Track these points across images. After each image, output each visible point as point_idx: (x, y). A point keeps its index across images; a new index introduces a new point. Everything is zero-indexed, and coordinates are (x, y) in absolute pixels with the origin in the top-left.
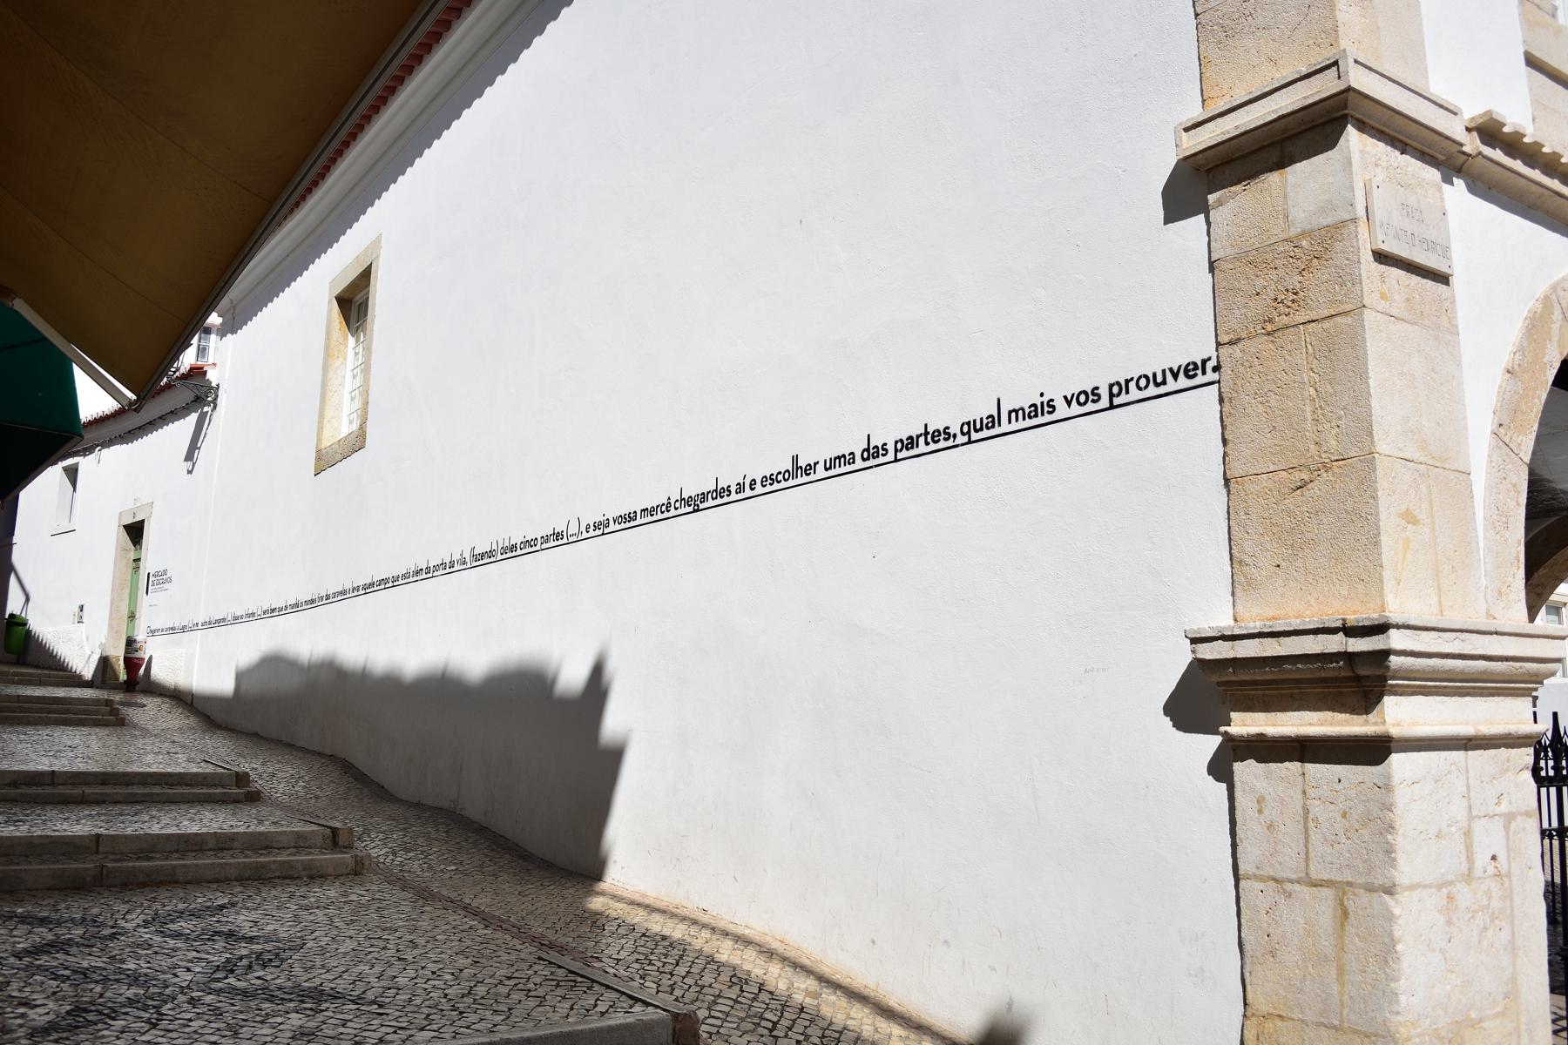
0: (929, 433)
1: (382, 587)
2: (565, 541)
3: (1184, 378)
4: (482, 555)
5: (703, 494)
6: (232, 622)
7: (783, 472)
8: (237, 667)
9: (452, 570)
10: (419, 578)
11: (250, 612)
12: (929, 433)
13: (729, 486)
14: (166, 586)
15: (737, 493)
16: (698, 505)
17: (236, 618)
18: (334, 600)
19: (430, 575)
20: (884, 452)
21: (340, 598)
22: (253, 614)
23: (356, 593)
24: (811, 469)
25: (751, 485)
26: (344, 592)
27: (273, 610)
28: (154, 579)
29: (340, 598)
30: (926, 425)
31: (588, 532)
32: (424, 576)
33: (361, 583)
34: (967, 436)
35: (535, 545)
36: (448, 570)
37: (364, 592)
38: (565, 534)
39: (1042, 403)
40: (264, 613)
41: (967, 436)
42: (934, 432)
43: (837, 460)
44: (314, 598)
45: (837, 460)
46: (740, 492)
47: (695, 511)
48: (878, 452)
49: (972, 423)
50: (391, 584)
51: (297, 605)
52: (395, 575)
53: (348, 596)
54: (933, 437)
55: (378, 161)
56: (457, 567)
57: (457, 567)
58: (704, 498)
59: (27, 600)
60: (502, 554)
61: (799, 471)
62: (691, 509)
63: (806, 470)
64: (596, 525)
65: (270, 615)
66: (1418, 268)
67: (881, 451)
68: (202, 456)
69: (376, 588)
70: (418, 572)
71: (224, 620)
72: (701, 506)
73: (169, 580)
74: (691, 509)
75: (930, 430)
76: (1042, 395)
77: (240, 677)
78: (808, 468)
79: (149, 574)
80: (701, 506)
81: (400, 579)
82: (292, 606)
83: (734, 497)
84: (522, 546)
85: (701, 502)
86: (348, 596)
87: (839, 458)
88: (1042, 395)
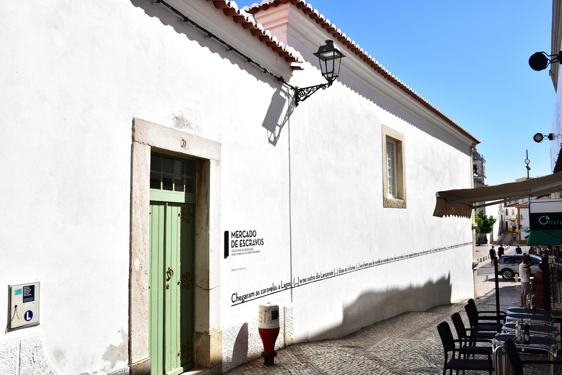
1: (415, 256)
2: (334, 275)
4: (435, 250)
5: (245, 295)
6: (339, 274)
8: (344, 304)
9: (374, 265)
10: (425, 254)
11: (352, 266)
14: (256, 248)
15: (256, 295)
16: (244, 300)
18: (398, 260)
19: (426, 253)
21: (401, 259)
22: (354, 268)
23: (407, 257)
25: (301, 281)
26: (402, 257)
27: (366, 265)
28: (234, 239)
29: (401, 259)
31: (301, 283)
32: (425, 254)
33: (409, 254)
35: (314, 279)
36: (430, 253)
37: (409, 257)
40: (361, 267)
46: (246, 298)
47: (243, 302)
48: (275, 288)
50: (417, 255)
51: (379, 262)
52: (370, 262)
53: (404, 258)
55: (381, 90)
56: (431, 252)
57: (431, 252)
58: (246, 297)
60: (339, 273)
62: (241, 302)
64: (258, 294)
65: (364, 267)
68: (550, 149)
69: (413, 256)
70: (424, 252)
72: (245, 300)
73: (261, 242)
74: (241, 302)
77: (346, 311)
79: (226, 233)
80: (245, 300)
81: (344, 271)
82: (377, 262)
83: (394, 260)
84: (262, 292)
85: (245, 299)
86: (404, 258)
87: (252, 293)
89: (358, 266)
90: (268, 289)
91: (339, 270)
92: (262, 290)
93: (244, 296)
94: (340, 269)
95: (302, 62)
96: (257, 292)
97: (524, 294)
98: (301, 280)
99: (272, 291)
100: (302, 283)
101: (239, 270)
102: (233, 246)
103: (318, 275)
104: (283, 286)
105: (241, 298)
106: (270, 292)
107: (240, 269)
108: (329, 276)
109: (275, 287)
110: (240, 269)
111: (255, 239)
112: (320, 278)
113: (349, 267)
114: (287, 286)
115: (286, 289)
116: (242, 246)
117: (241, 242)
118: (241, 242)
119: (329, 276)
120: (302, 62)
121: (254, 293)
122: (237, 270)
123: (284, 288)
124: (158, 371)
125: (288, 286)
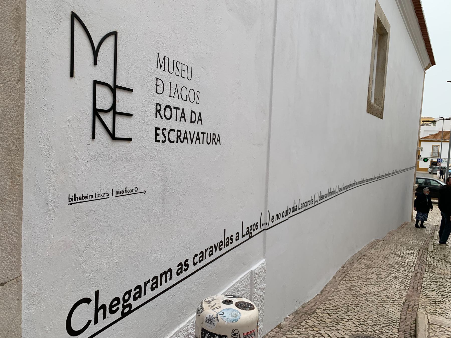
0: (83, 197)
3: (234, 305)
5: (156, 278)
7: (256, 229)
11: (332, 191)
12: (83, 197)
13: (187, 260)
17: (321, 197)
20: (186, 268)
24: (86, 197)
30: (83, 195)
34: (70, 198)
38: (259, 224)
39: (119, 191)
41: (70, 198)
42: (85, 197)
43: (164, 276)
44: (362, 180)
45: (164, 276)
48: (228, 242)
49: (74, 200)
54: (85, 198)
59: (187, 88)
61: (77, 198)
63: (79, 198)
64: (230, 241)
66: (384, 81)
67: (184, 267)
71: (312, 201)
75: (84, 196)
76: (88, 194)
78: (221, 244)
84: (197, 259)
87: (165, 273)
88: (88, 194)
89: (316, 199)
90: (212, 247)
91: (319, 196)
92: (196, 255)
93: (133, 293)
94: (321, 194)
95: (184, 78)
96: (181, 264)
97: (168, 330)
98: (273, 216)
99: (220, 249)
100: (275, 223)
101: (112, 198)
102: (193, 120)
103: (295, 205)
104: (300, 207)
105: (222, 245)
106: (219, 253)
107: (119, 193)
108: (309, 206)
109: (228, 238)
110: (119, 193)
111: (213, 144)
112: (298, 211)
113: (330, 192)
114: (252, 231)
115: (250, 237)
116: (159, 141)
117: (158, 131)
118: (158, 131)
119: (309, 206)
120: (184, 78)
121: (170, 270)
122: (104, 196)
123: (247, 237)
124: (168, 66)
125: (254, 230)
